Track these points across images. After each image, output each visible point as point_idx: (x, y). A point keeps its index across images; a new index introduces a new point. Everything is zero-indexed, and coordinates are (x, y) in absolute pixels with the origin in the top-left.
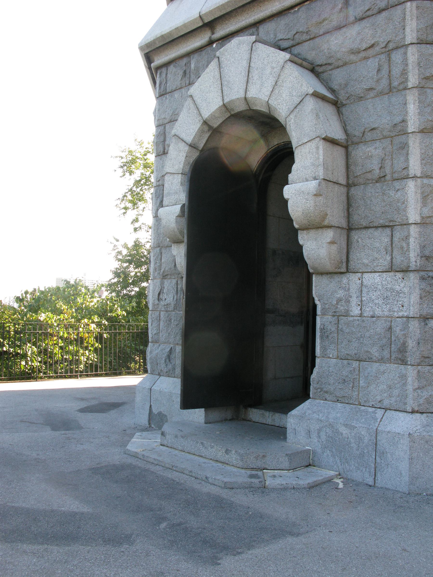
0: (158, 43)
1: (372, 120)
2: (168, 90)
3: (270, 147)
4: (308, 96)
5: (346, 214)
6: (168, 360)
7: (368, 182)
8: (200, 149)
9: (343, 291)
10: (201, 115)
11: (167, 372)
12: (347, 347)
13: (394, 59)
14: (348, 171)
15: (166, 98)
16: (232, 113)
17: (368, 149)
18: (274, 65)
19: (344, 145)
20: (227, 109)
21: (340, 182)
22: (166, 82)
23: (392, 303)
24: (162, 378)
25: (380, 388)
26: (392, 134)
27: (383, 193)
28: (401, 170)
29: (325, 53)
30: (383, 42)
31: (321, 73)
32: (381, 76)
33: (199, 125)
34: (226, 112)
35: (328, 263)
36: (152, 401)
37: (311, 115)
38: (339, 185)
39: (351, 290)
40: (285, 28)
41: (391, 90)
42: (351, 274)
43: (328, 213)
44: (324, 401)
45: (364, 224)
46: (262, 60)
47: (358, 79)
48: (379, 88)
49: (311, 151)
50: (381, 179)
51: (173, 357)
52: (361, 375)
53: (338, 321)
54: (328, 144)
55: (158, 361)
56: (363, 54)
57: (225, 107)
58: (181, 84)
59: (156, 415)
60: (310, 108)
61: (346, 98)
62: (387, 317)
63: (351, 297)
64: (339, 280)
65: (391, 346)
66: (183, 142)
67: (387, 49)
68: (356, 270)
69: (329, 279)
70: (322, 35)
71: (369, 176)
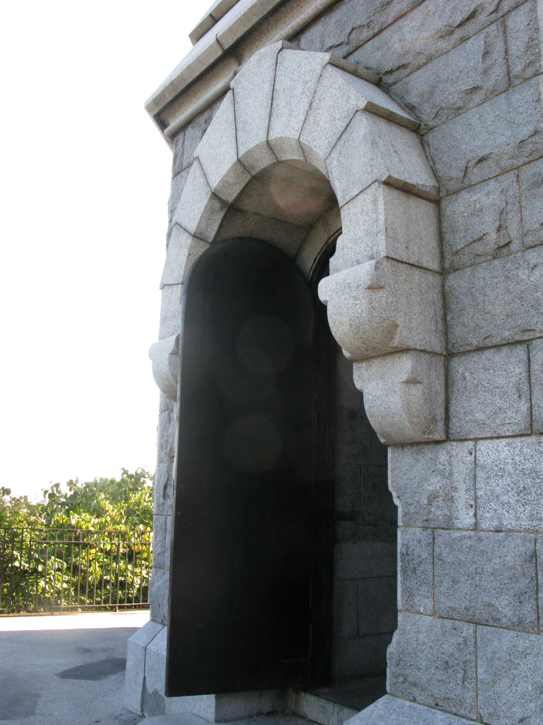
0: (168, 96)
1: (479, 143)
3: (332, 234)
4: (359, 113)
5: (440, 326)
7: (478, 260)
8: (211, 240)
9: (439, 479)
10: (208, 184)
12: (451, 593)
13: (512, 26)
14: (442, 245)
15: (182, 177)
16: (254, 173)
17: (474, 198)
18: (308, 78)
19: (431, 197)
20: (245, 168)
21: (425, 265)
22: (183, 154)
23: (535, 502)
25: (519, 688)
26: (517, 163)
27: (507, 277)
28: (538, 226)
29: (395, 49)
30: (490, 4)
31: (391, 85)
32: (492, 62)
33: (205, 201)
35: (407, 423)
36: (146, 669)
37: (363, 145)
38: (423, 271)
39: (455, 476)
40: (336, 28)
41: (510, 83)
42: (454, 443)
43: (398, 322)
44: (411, 703)
45: (475, 343)
46: (291, 75)
47: (450, 77)
48: (489, 84)
49: (365, 208)
50: (502, 249)
52: (480, 654)
53: (434, 538)
54: (396, 194)
56: (458, 34)
57: (241, 164)
59: (151, 695)
60: (362, 133)
61: (434, 116)
62: (527, 530)
63: (455, 489)
64: (432, 456)
65: (537, 594)
66: (186, 232)
67: (500, 14)
68: (462, 435)
69: (414, 455)
70: (392, 24)
71: (479, 248)
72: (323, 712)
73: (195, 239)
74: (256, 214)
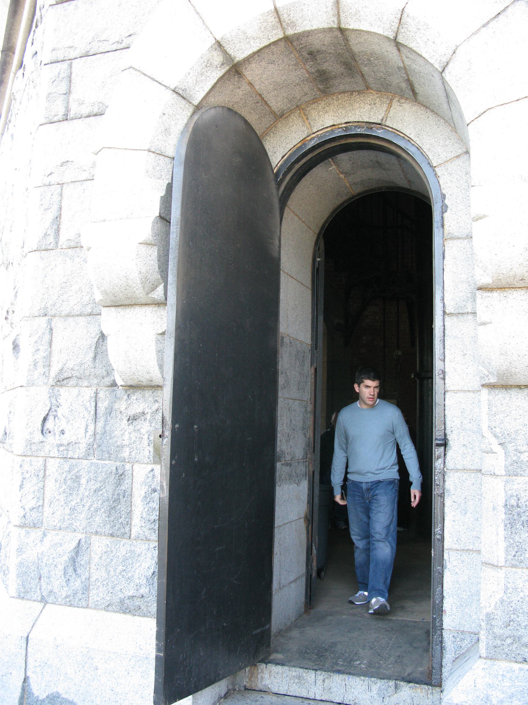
6: (70, 570)
8: (196, 102)
11: (66, 597)
16: (290, 32)
34: (274, 28)
44: (521, 665)
51: (82, 563)
55: (44, 572)
59: (43, 701)
72: (298, 683)
73: (175, 95)
74: (250, 84)
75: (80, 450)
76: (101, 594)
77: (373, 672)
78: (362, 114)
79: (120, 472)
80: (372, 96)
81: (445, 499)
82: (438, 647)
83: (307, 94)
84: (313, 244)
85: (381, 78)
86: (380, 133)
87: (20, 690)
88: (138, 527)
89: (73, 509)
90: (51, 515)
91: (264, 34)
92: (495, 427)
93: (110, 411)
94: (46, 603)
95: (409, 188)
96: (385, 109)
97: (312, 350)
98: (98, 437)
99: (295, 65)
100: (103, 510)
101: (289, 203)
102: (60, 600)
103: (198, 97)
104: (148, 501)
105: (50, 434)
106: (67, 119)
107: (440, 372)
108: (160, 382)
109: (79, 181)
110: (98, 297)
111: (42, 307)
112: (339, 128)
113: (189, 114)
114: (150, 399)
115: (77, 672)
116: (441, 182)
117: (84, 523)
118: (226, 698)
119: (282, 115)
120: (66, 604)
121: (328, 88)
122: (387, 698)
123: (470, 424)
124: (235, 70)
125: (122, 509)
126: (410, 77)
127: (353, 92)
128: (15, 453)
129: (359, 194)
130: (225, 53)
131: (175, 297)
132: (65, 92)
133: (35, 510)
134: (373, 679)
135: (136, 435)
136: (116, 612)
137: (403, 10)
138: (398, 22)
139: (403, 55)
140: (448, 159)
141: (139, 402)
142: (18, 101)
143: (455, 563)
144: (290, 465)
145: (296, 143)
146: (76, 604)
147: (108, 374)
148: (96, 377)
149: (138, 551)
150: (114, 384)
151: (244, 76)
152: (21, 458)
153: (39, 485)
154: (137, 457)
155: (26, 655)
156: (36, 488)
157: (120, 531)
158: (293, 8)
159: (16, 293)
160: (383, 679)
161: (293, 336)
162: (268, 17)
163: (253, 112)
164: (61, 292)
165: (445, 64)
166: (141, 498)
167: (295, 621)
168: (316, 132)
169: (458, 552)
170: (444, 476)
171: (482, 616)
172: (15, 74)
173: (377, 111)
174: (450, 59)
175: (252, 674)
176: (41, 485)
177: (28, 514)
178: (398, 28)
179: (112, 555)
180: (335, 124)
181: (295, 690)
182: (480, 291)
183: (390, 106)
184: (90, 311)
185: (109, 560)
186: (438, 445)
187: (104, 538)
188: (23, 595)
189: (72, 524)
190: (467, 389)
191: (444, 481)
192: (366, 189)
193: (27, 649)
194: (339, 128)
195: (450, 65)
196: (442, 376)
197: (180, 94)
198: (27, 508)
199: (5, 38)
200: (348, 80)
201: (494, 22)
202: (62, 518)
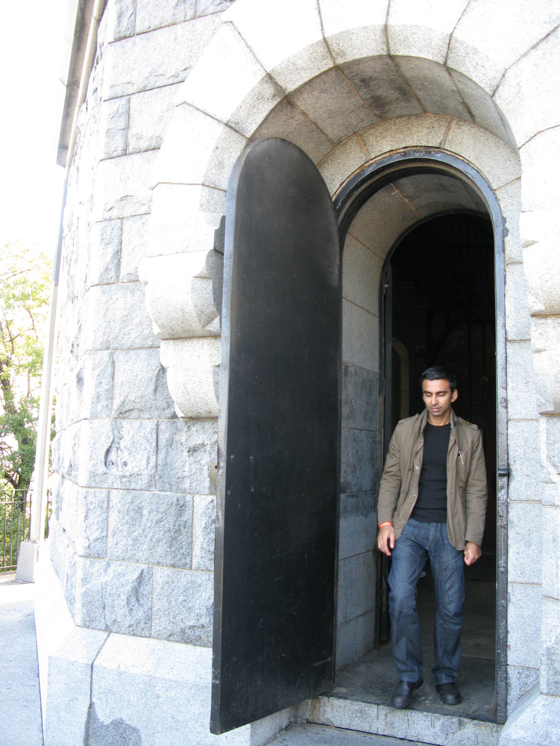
2: (138, 30)
6: (133, 600)
8: (249, 135)
11: (130, 626)
16: (340, 61)
20: (329, 51)
22: (134, 13)
24: (114, 637)
34: (324, 57)
36: (95, 693)
55: (108, 601)
58: (174, 15)
59: (108, 726)
72: (360, 717)
73: (228, 129)
74: (304, 113)
75: (142, 481)
76: (163, 624)
77: (437, 707)
78: (420, 138)
79: (181, 503)
80: (430, 120)
81: (509, 531)
82: (503, 683)
83: (363, 120)
84: (380, 270)
85: (437, 101)
86: (438, 157)
87: (86, 716)
88: (199, 557)
89: (136, 540)
90: (114, 545)
91: (314, 64)
92: (554, 457)
93: (171, 443)
94: (110, 632)
95: (477, 210)
96: (443, 132)
97: (380, 380)
98: (159, 468)
99: (348, 93)
100: (164, 541)
101: (351, 229)
102: (123, 629)
103: (251, 129)
104: (208, 532)
105: (113, 466)
106: (126, 154)
107: (503, 401)
108: (215, 413)
109: (138, 215)
110: (156, 330)
111: (105, 340)
112: (397, 153)
113: (242, 147)
114: (210, 430)
115: (140, 699)
116: (502, 205)
117: (147, 554)
118: (287, 730)
119: (339, 142)
120: (129, 634)
121: (384, 113)
122: (451, 735)
123: (533, 454)
124: (287, 101)
125: (183, 539)
126: (466, 100)
127: (411, 115)
128: (80, 485)
129: (426, 218)
130: (276, 84)
131: (229, 330)
132: (123, 127)
133: (99, 540)
134: (436, 715)
135: (196, 466)
136: (178, 642)
137: (451, 34)
138: (447, 47)
139: (454, 79)
140: (508, 181)
141: (199, 433)
142: (82, 134)
143: (519, 597)
144: (357, 496)
145: (354, 170)
146: (139, 634)
147: (168, 406)
148: (157, 409)
149: (199, 581)
150: (174, 416)
151: (297, 106)
152: (85, 490)
153: (103, 516)
154: (198, 488)
155: (91, 682)
156: (100, 519)
157: (181, 562)
158: (342, 38)
159: (80, 326)
160: (447, 715)
161: (358, 365)
162: (317, 48)
163: (308, 140)
164: (122, 326)
165: (495, 87)
166: (201, 529)
167: (363, 656)
168: (374, 158)
169: (522, 585)
170: (507, 507)
171: (542, 651)
172: (80, 107)
173: (435, 135)
174: (500, 83)
175: (314, 707)
176: (104, 516)
177: (92, 544)
178: (447, 53)
179: (174, 585)
180: (393, 149)
181: (357, 724)
182: (534, 318)
183: (448, 128)
184: (151, 343)
185: (170, 590)
186: (502, 475)
187: (166, 568)
188: (88, 624)
189: (135, 554)
190: (530, 418)
191: (508, 512)
192: (434, 212)
193: (92, 676)
194: (397, 153)
195: (501, 88)
196: (504, 404)
197: (232, 127)
198: (91, 538)
199: (69, 73)
200: (403, 104)
201: (544, 43)
202: (125, 549)
